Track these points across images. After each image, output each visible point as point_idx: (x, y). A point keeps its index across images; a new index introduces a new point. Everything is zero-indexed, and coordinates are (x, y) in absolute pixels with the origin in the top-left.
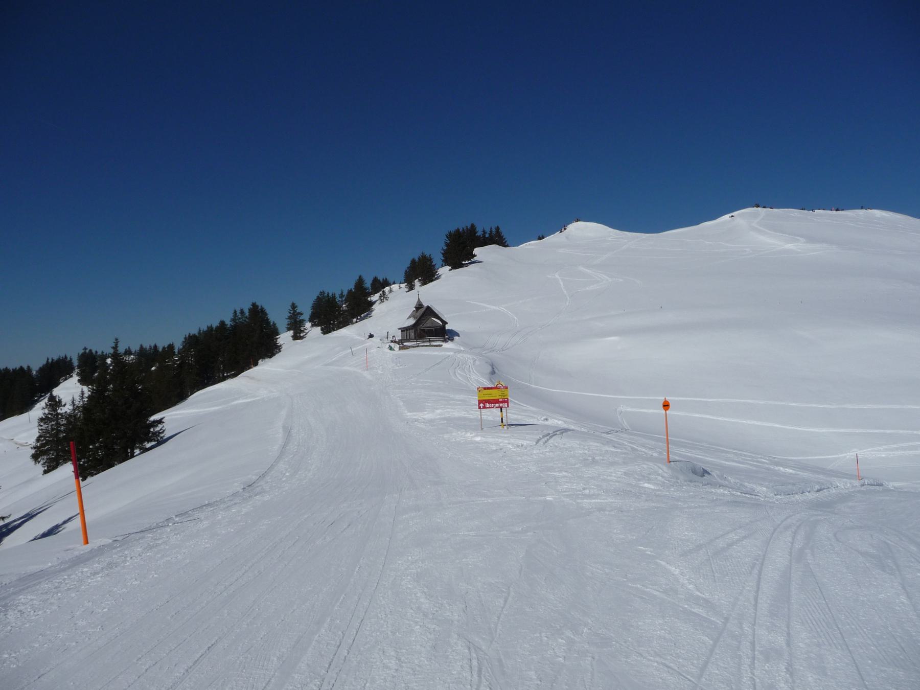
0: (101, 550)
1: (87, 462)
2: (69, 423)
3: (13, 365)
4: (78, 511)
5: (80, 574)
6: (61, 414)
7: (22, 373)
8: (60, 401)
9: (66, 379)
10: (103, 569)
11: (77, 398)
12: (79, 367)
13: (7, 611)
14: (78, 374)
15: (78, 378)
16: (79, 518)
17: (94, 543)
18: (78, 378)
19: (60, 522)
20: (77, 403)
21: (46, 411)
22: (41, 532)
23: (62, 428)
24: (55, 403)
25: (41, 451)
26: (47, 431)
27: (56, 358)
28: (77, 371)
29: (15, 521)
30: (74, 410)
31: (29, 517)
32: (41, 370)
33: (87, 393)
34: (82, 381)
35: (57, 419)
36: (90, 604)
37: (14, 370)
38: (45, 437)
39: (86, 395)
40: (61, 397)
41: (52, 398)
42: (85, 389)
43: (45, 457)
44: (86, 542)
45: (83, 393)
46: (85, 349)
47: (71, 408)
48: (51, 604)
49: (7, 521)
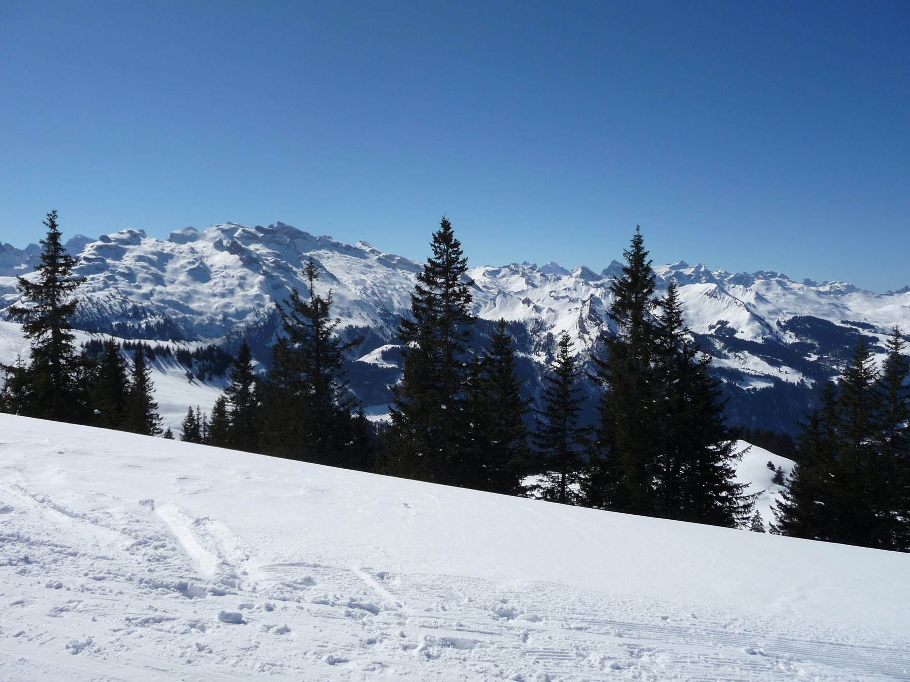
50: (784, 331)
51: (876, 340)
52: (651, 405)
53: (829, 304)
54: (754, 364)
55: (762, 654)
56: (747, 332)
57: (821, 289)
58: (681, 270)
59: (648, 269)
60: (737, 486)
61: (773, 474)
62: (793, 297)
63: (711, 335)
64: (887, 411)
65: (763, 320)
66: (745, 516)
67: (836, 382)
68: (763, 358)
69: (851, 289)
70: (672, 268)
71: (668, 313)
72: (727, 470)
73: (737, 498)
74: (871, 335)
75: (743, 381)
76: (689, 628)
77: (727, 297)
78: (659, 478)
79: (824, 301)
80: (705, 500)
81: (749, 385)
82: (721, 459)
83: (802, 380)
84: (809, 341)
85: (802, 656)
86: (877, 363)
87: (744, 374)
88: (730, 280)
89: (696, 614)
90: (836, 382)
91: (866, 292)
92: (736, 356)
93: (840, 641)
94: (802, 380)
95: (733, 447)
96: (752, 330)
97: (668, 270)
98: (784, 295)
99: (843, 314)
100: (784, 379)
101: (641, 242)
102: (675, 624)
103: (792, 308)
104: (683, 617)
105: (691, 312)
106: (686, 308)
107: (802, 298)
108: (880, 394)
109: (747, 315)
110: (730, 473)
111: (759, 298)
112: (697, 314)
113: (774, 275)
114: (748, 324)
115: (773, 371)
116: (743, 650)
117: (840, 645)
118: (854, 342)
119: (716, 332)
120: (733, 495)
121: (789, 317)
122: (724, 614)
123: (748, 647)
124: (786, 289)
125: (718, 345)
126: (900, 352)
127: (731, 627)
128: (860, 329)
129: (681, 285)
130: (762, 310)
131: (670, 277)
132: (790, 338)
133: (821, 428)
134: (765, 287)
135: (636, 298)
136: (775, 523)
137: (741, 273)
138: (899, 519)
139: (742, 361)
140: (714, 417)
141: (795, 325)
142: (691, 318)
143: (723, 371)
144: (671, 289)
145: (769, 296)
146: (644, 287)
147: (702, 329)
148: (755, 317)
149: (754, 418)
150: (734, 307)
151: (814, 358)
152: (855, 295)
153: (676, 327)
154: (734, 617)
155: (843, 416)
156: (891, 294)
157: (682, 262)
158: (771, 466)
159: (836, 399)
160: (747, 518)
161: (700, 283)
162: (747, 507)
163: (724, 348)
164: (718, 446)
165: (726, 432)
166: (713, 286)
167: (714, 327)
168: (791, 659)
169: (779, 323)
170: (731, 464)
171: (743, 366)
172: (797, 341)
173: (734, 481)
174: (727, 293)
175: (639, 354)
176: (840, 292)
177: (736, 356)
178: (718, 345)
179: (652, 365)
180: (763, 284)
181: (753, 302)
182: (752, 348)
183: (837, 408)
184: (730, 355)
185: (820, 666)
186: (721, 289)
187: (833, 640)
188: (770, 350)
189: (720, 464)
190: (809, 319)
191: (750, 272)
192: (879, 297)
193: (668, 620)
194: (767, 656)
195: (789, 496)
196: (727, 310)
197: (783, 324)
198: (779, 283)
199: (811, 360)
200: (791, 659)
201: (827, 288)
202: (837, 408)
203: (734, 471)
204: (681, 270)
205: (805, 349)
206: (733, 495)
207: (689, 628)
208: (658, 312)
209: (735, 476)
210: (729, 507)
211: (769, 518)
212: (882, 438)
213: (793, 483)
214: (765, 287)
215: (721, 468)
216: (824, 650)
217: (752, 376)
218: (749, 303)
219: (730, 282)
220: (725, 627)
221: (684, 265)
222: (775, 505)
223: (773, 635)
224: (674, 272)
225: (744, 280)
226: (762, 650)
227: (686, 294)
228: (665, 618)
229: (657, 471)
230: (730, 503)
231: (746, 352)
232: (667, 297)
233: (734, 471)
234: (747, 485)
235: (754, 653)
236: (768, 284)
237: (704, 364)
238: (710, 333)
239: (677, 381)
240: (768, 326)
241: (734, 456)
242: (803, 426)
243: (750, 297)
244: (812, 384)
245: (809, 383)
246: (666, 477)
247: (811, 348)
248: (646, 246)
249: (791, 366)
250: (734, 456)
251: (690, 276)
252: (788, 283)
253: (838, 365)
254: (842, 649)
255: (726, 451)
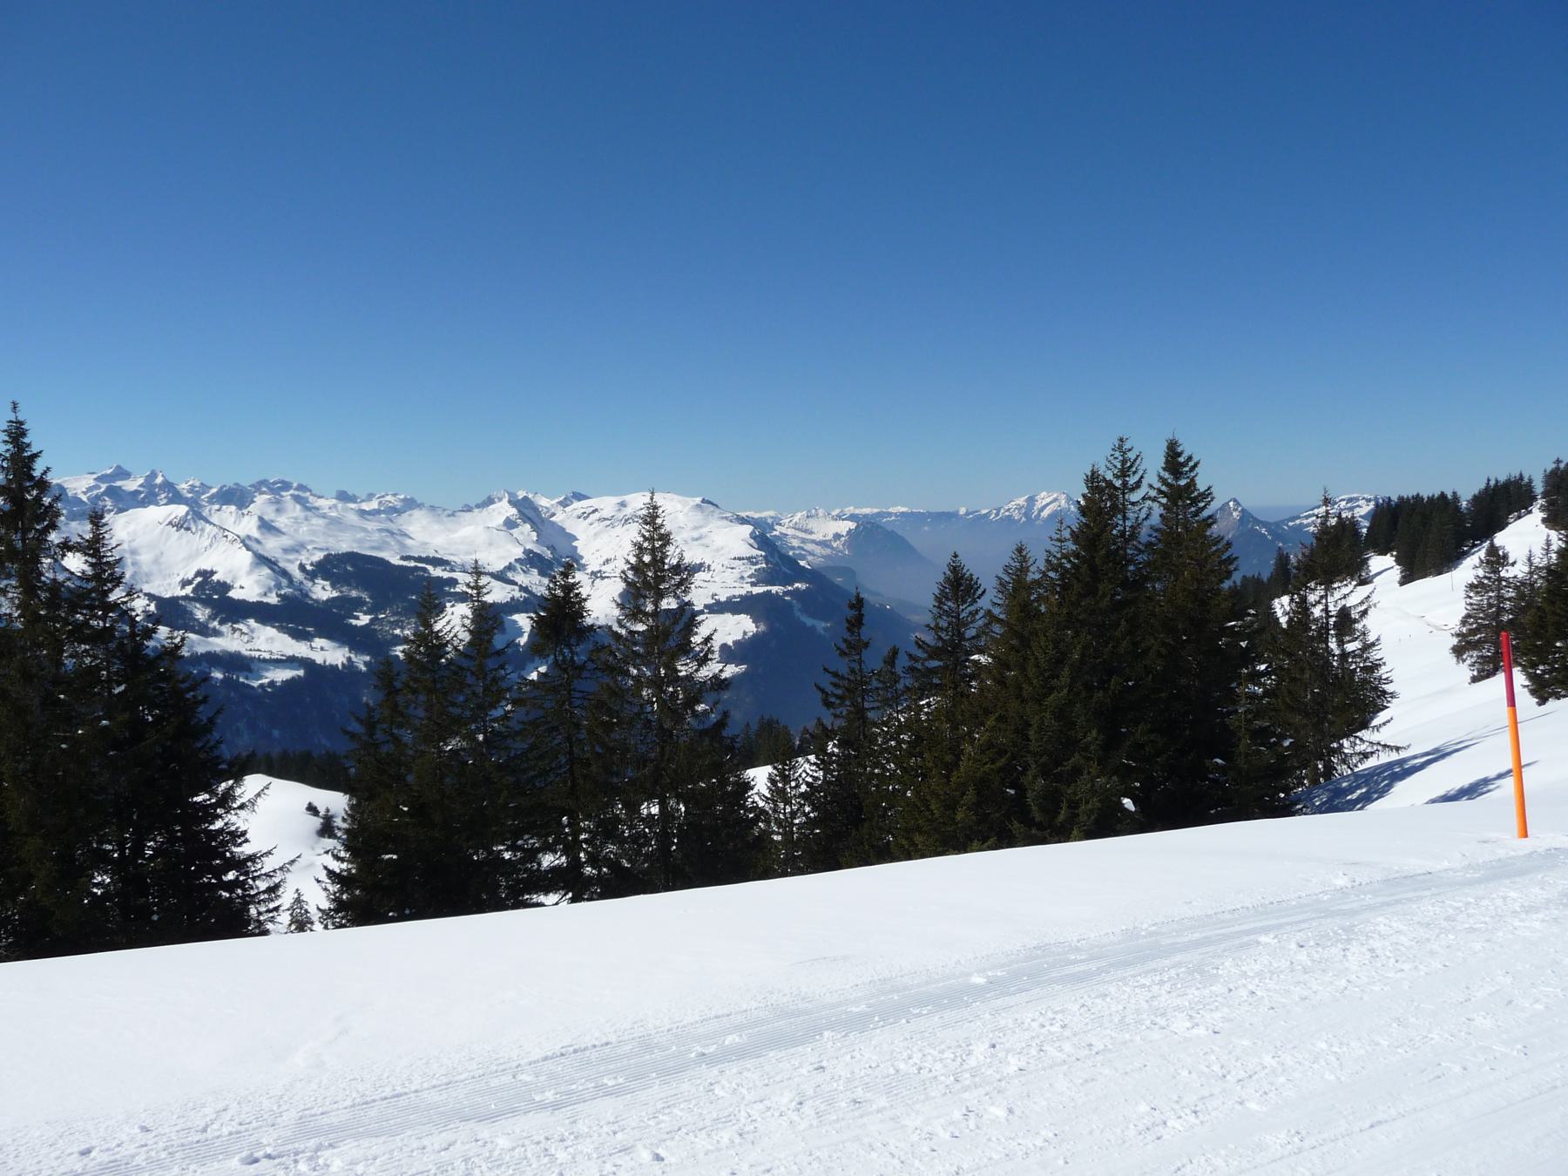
0: (1552, 857)
1: (1550, 672)
2: (1521, 596)
3: (1428, 490)
4: (1509, 764)
5: (1499, 902)
6: (1506, 580)
7: (1444, 504)
8: (1505, 557)
9: (1519, 517)
10: (1549, 901)
11: (1538, 553)
12: (1545, 495)
13: (1349, 941)
14: (1542, 509)
15: (1542, 515)
16: (1509, 783)
17: (1543, 837)
18: (1542, 515)
19: (1492, 774)
20: (1536, 561)
21: (1481, 573)
22: (1441, 792)
23: (1508, 605)
24: (1497, 559)
25: (1469, 643)
26: (1480, 609)
27: (1502, 478)
28: (1541, 502)
29: (1415, 757)
30: (1531, 573)
31: (1438, 755)
32: (1476, 499)
33: (1557, 544)
34: (1551, 521)
35: (1499, 589)
36: (1509, 980)
37: (1431, 499)
38: (1476, 618)
39: (1554, 547)
40: (1508, 549)
41: (1493, 550)
42: (1554, 535)
43: (1475, 653)
44: (1525, 834)
45: (1548, 543)
46: (1558, 461)
47: (1526, 569)
48: (1432, 953)
49: (1403, 755)
50: (312, 580)
51: (454, 582)
52: (75, 742)
53: (380, 530)
54: (267, 641)
55: (269, 1157)
56: (249, 586)
57: (366, 507)
58: (118, 483)
59: (42, 485)
60: (252, 858)
61: (317, 822)
62: (321, 522)
63: (186, 598)
64: (474, 693)
65: (275, 563)
66: (272, 906)
67: (401, 656)
68: (281, 629)
69: (410, 504)
70: (100, 479)
71: (92, 565)
72: (231, 833)
73: (254, 879)
74: (446, 575)
75: (250, 670)
76: (133, 1156)
77: (208, 528)
78: (106, 872)
79: (371, 525)
80: (203, 899)
81: (261, 677)
82: (220, 816)
83: (349, 659)
84: (354, 594)
85: (334, 1137)
86: (455, 621)
87: (252, 659)
88: (213, 496)
89: (149, 1123)
90: (401, 656)
91: (433, 508)
92: (234, 630)
93: (399, 1090)
94: (349, 659)
95: (238, 791)
96: (258, 582)
97: (92, 483)
98: (306, 519)
99: (403, 546)
100: (319, 661)
101: (24, 434)
102: (106, 1157)
103: (321, 541)
104: (124, 1137)
105: (145, 558)
106: (134, 552)
107: (336, 523)
108: (461, 668)
109: (247, 557)
110: (238, 836)
111: (266, 526)
112: (156, 561)
113: (286, 486)
114: (250, 572)
115: (300, 649)
116: (235, 1162)
117: (397, 1096)
118: (418, 589)
119: (194, 590)
120: (246, 874)
121: (318, 556)
122: (203, 1106)
123: (244, 1154)
124: (309, 509)
125: (201, 613)
126: (489, 599)
127: (215, 1126)
128: (430, 568)
129: (121, 511)
130: (272, 546)
131: (98, 497)
132: (322, 591)
133: (379, 735)
134: (274, 507)
135: (23, 540)
136: (326, 905)
137: (230, 483)
138: (507, 856)
139: (246, 638)
140: (199, 745)
141: (329, 567)
142: (145, 569)
143: (214, 659)
144: (96, 519)
145: (282, 522)
146: (40, 519)
147: (170, 589)
148: (262, 560)
149: (276, 733)
150: (223, 545)
151: (364, 620)
152: (417, 513)
153: (111, 590)
154: (221, 1106)
155: (411, 711)
156: (469, 509)
157: (119, 467)
158: (312, 809)
159: (398, 685)
160: (276, 909)
161: (157, 504)
162: (273, 889)
163: (212, 617)
164: (213, 793)
165: (224, 766)
166: (181, 510)
167: (189, 582)
168: (318, 1148)
169: (302, 567)
170: (238, 820)
171: (249, 646)
172: (335, 594)
173: (246, 850)
174: (208, 521)
175: (40, 646)
176: (394, 510)
177: (234, 630)
178: (201, 613)
179: (69, 663)
180: (270, 502)
181: (255, 534)
182: (262, 612)
183: (400, 699)
184: (225, 628)
185: (365, 1142)
186: (197, 514)
187: (388, 1092)
188: (293, 614)
189: (219, 824)
190: (352, 557)
191: (246, 482)
192: (453, 515)
193: (93, 1154)
194: (280, 1156)
195: (342, 854)
196: (210, 551)
197: (309, 568)
198: (297, 499)
199: (359, 623)
200: (318, 1148)
201: (374, 505)
202: (400, 699)
203: (244, 833)
204: (118, 483)
205: (347, 606)
206: (246, 874)
207: (133, 1156)
208: (75, 563)
209: (247, 841)
210: (244, 896)
211: (318, 899)
212: (471, 737)
213: (347, 831)
214: (274, 507)
215: (221, 831)
216: (373, 1113)
217: (265, 661)
218: (249, 537)
219: (211, 500)
220: (204, 1130)
221: (122, 473)
222: (323, 876)
223: (290, 1117)
224: (104, 487)
225: (236, 497)
226: (269, 1150)
227: (131, 528)
228: (86, 1153)
229: (101, 860)
230: (244, 890)
231: (251, 622)
232: (88, 536)
233: (244, 833)
234: (269, 853)
235: (256, 1161)
236: (278, 502)
237: (172, 653)
238: (183, 593)
239: (122, 688)
240: (285, 573)
241: (242, 807)
242: (353, 736)
243: (249, 526)
244: (366, 664)
245: (361, 661)
246: (118, 868)
247: (357, 604)
248: (35, 440)
249: (329, 637)
250: (242, 807)
251: (137, 493)
252: (311, 499)
253: (403, 628)
254: (403, 1101)
255: (226, 800)
